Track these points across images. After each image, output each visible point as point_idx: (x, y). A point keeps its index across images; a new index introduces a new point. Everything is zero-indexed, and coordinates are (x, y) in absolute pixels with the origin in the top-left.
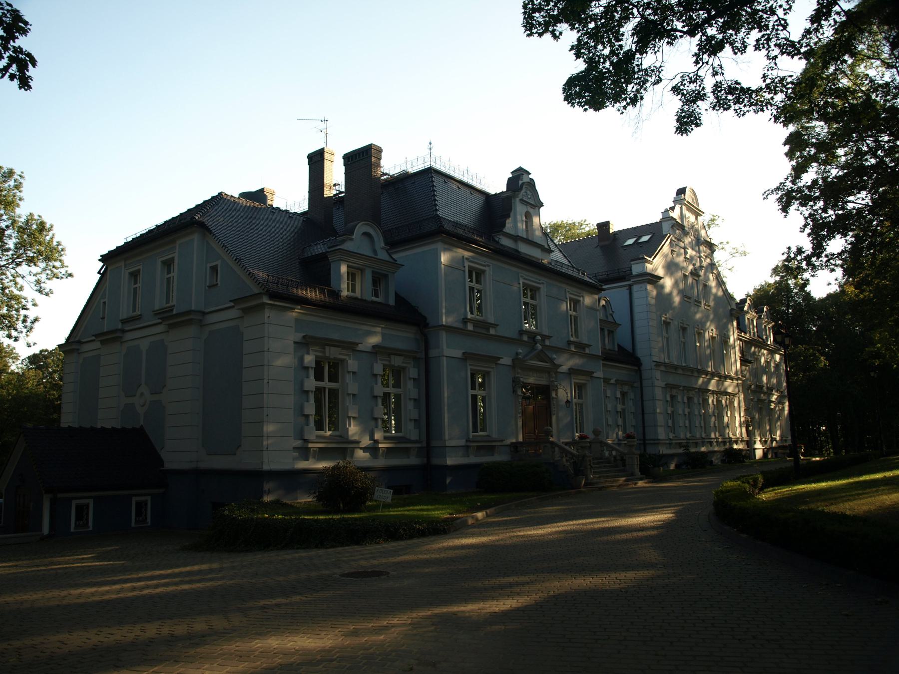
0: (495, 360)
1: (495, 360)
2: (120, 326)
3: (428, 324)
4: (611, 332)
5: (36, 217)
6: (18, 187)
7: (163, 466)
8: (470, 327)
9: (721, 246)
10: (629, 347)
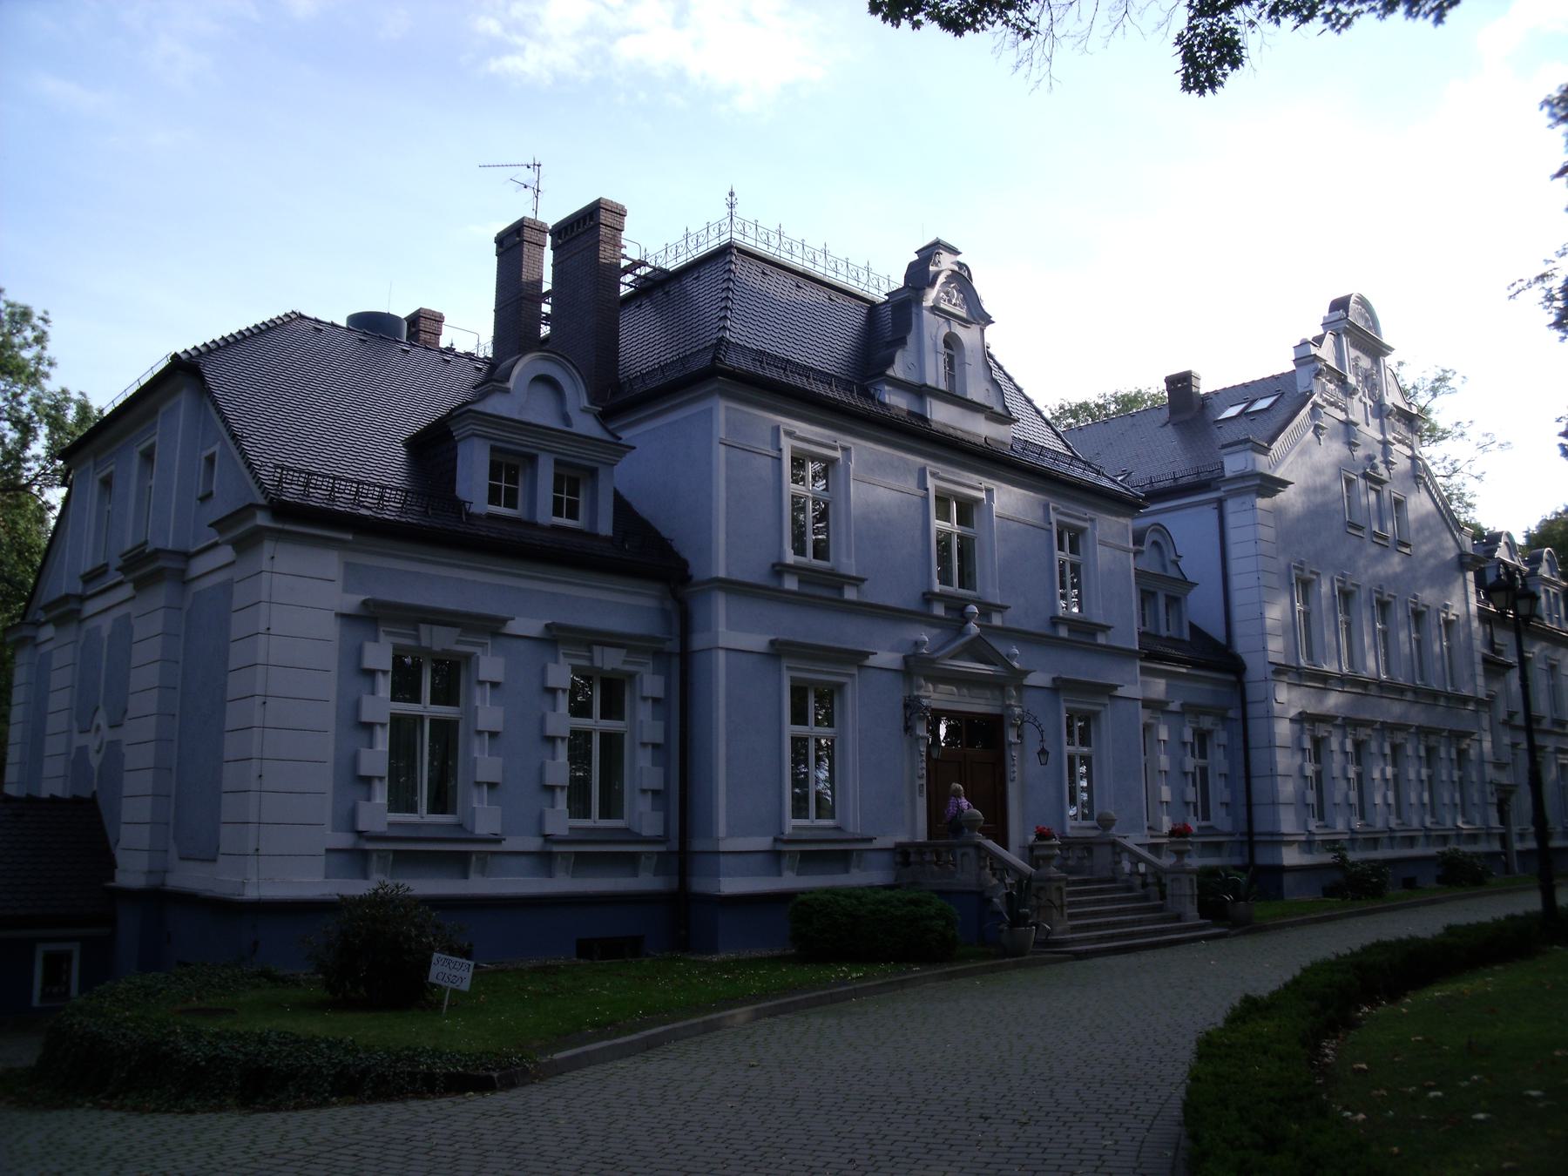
0: (857, 658)
1: (857, 658)
2: (78, 588)
3: (690, 578)
4: (1174, 602)
5: (75, 396)
6: (40, 339)
7: (112, 878)
8: (791, 583)
9: (1458, 430)
10: (1218, 633)
